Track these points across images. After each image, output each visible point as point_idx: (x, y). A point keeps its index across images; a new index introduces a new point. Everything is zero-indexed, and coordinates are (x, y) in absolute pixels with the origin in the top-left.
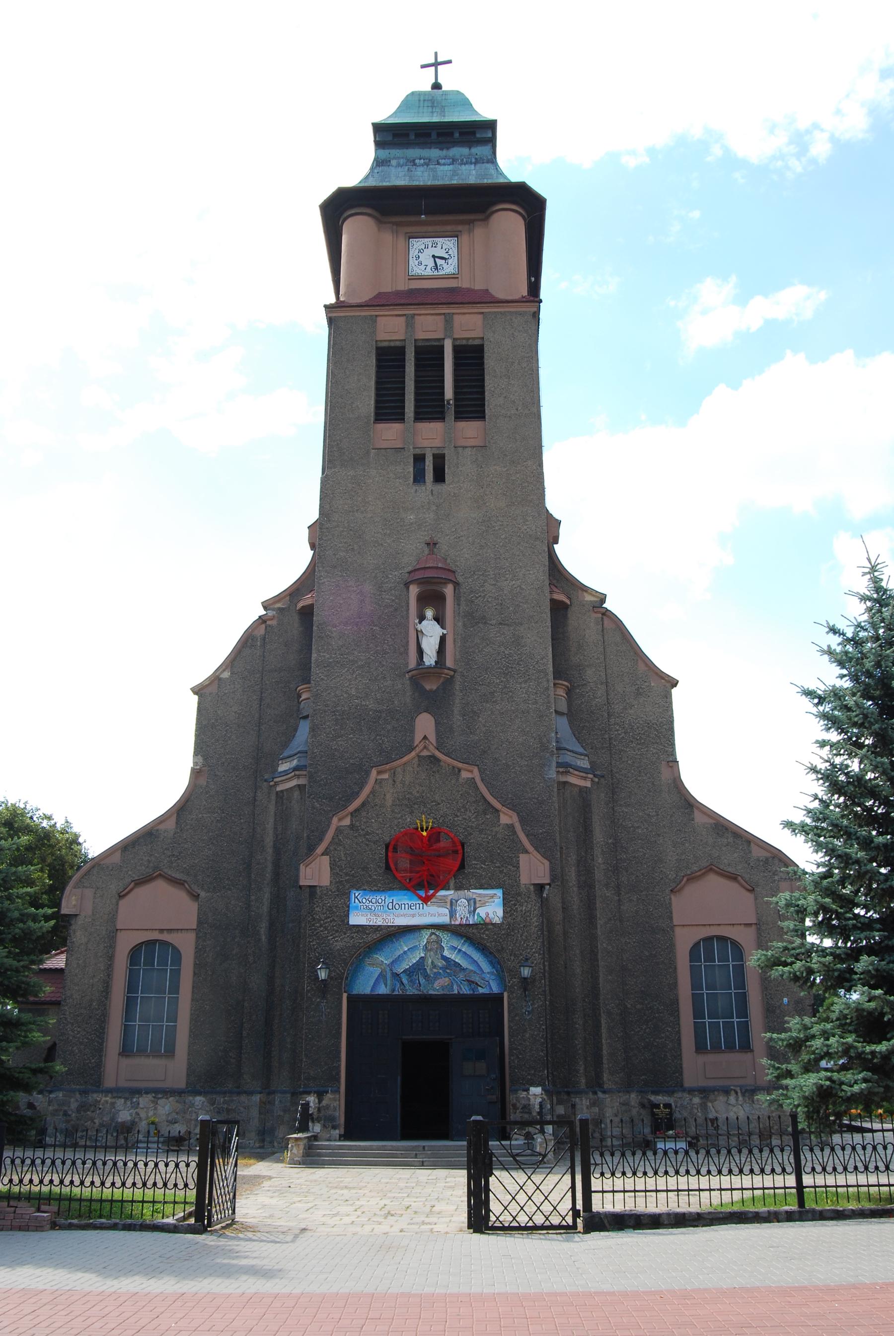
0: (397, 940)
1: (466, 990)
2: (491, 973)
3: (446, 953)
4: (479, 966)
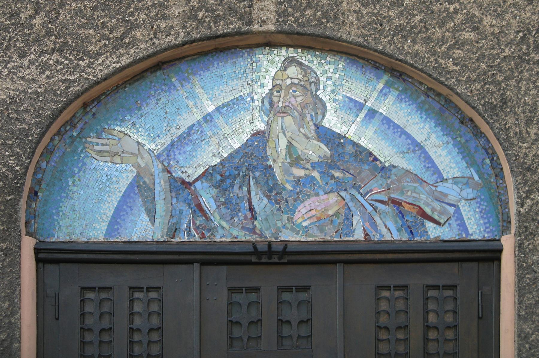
0: (184, 80)
1: (389, 230)
2: (467, 182)
3: (332, 121)
4: (428, 158)
